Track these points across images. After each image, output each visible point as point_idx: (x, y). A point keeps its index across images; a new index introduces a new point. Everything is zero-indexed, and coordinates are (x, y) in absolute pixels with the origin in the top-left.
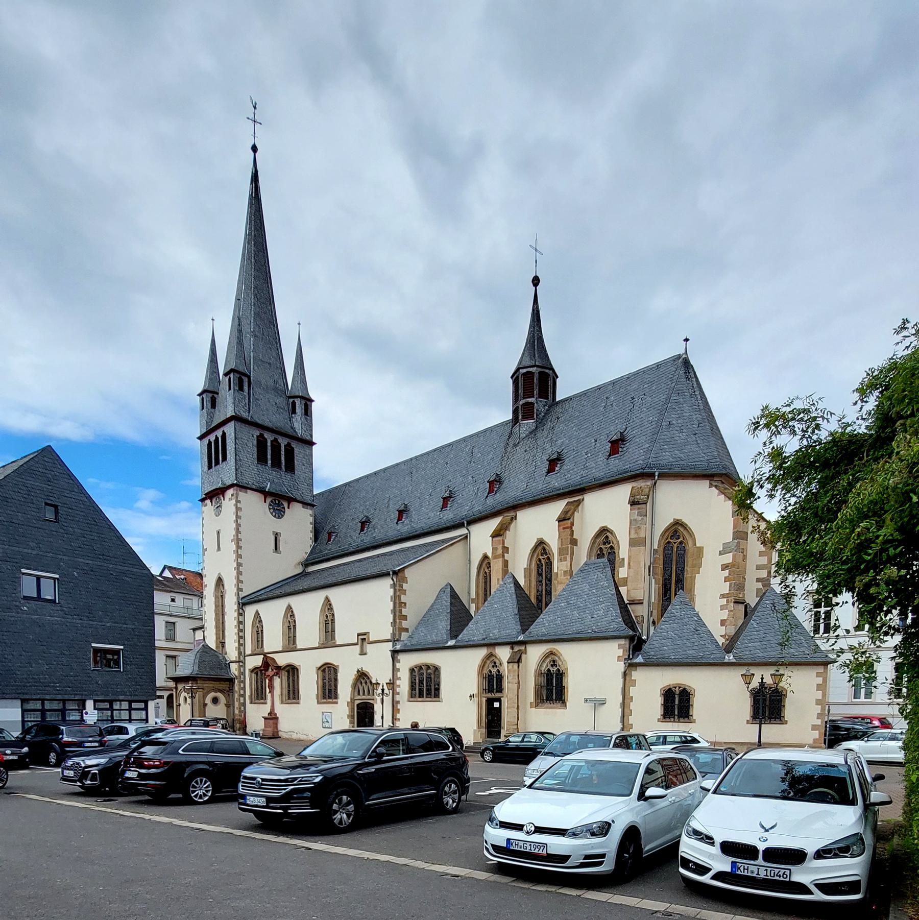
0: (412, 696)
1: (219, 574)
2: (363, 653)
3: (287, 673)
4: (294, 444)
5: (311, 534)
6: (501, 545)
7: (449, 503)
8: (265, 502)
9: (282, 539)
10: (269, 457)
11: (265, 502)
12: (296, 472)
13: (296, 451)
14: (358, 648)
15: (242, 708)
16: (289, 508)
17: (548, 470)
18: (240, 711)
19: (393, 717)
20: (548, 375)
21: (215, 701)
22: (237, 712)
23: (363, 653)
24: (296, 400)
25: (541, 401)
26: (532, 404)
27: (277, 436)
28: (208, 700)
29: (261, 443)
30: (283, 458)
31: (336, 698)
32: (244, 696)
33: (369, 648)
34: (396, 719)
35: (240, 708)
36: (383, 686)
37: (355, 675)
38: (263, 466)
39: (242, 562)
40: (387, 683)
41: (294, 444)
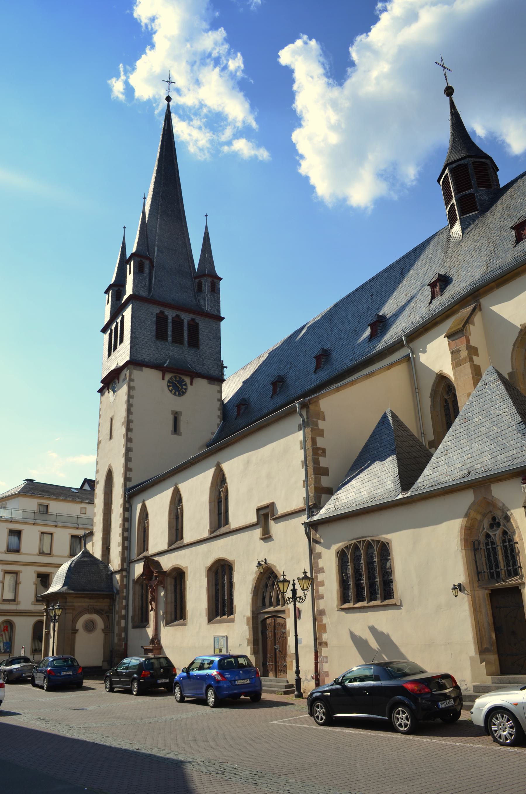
0: (344, 598)
1: (110, 466)
2: (267, 537)
3: (173, 581)
4: (199, 320)
5: (220, 412)
6: (465, 345)
7: (378, 328)
8: (163, 379)
9: (183, 420)
10: (170, 333)
11: (163, 379)
12: (201, 347)
13: (201, 327)
14: (258, 532)
15: (123, 635)
16: (191, 384)
17: (516, 241)
18: (120, 640)
19: (315, 640)
20: (486, 164)
21: (90, 627)
22: (116, 640)
23: (267, 537)
24: (202, 280)
25: (483, 190)
26: (472, 195)
27: (178, 313)
28: (80, 624)
29: (161, 320)
30: (186, 334)
31: (231, 612)
32: (125, 617)
33: (275, 528)
34: (321, 644)
35: (120, 635)
36: (294, 585)
37: (256, 573)
38: (163, 343)
39: (132, 446)
40: (298, 579)
41: (199, 320)
